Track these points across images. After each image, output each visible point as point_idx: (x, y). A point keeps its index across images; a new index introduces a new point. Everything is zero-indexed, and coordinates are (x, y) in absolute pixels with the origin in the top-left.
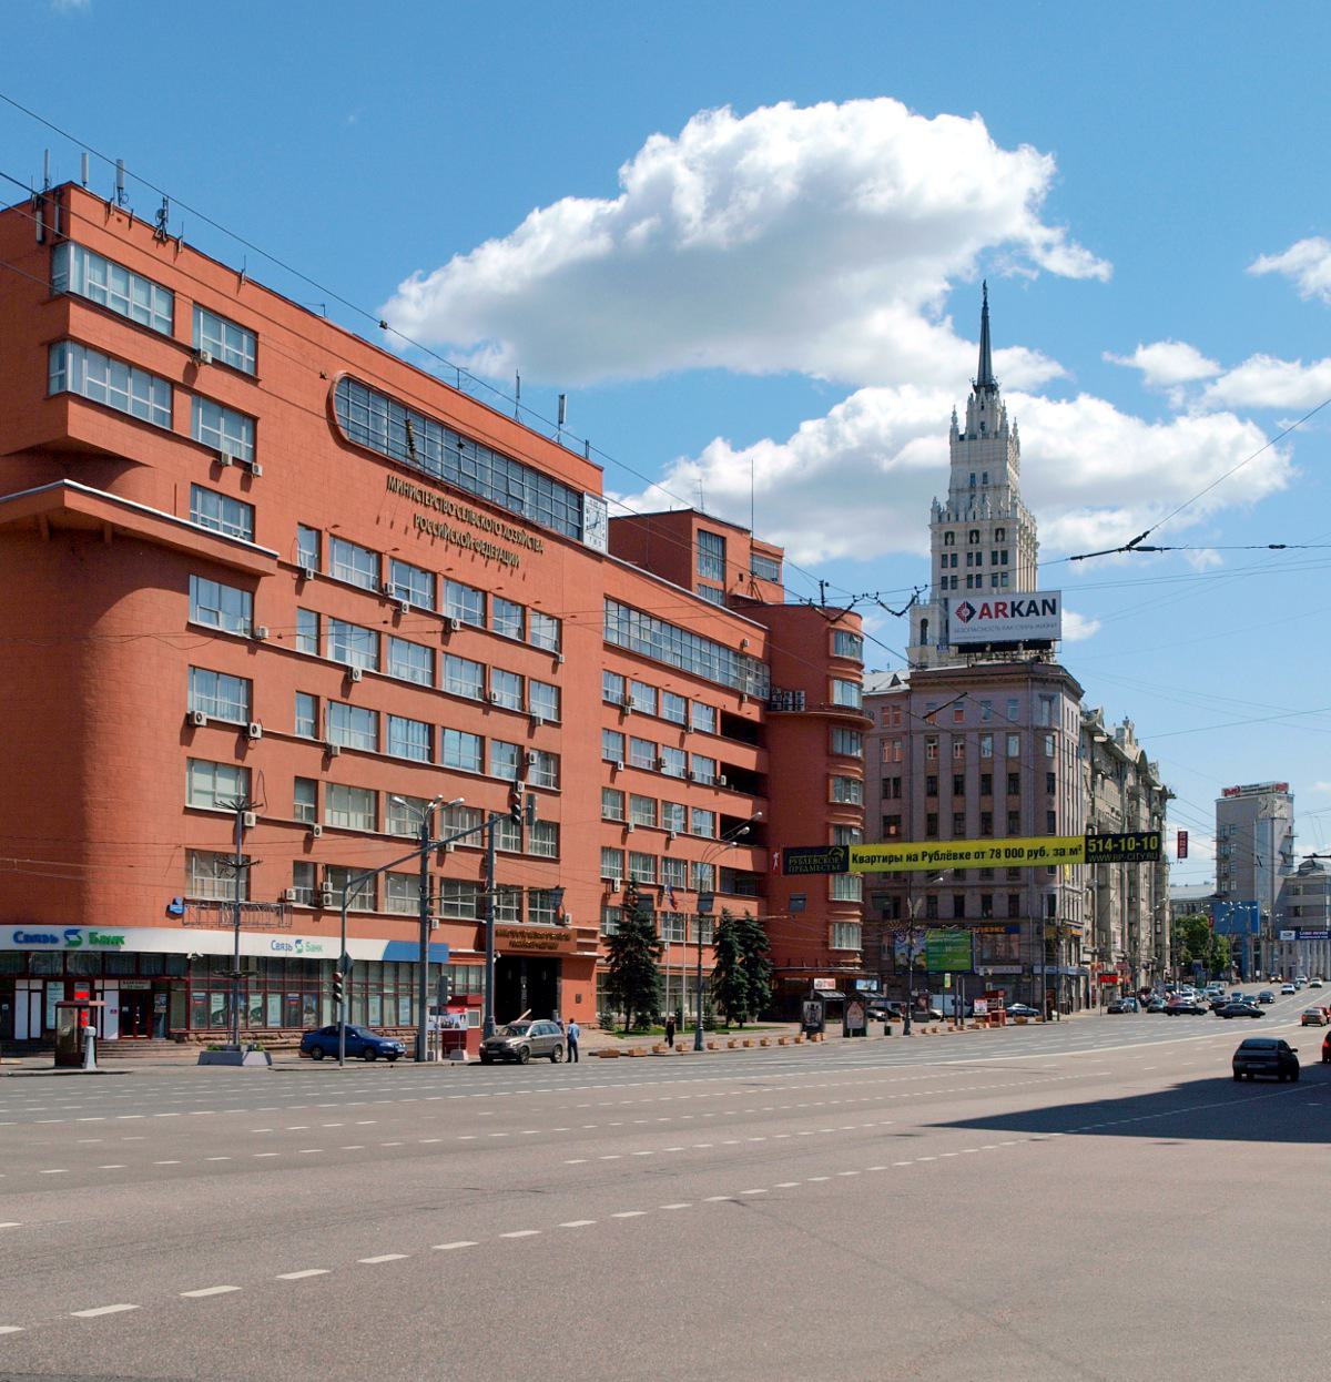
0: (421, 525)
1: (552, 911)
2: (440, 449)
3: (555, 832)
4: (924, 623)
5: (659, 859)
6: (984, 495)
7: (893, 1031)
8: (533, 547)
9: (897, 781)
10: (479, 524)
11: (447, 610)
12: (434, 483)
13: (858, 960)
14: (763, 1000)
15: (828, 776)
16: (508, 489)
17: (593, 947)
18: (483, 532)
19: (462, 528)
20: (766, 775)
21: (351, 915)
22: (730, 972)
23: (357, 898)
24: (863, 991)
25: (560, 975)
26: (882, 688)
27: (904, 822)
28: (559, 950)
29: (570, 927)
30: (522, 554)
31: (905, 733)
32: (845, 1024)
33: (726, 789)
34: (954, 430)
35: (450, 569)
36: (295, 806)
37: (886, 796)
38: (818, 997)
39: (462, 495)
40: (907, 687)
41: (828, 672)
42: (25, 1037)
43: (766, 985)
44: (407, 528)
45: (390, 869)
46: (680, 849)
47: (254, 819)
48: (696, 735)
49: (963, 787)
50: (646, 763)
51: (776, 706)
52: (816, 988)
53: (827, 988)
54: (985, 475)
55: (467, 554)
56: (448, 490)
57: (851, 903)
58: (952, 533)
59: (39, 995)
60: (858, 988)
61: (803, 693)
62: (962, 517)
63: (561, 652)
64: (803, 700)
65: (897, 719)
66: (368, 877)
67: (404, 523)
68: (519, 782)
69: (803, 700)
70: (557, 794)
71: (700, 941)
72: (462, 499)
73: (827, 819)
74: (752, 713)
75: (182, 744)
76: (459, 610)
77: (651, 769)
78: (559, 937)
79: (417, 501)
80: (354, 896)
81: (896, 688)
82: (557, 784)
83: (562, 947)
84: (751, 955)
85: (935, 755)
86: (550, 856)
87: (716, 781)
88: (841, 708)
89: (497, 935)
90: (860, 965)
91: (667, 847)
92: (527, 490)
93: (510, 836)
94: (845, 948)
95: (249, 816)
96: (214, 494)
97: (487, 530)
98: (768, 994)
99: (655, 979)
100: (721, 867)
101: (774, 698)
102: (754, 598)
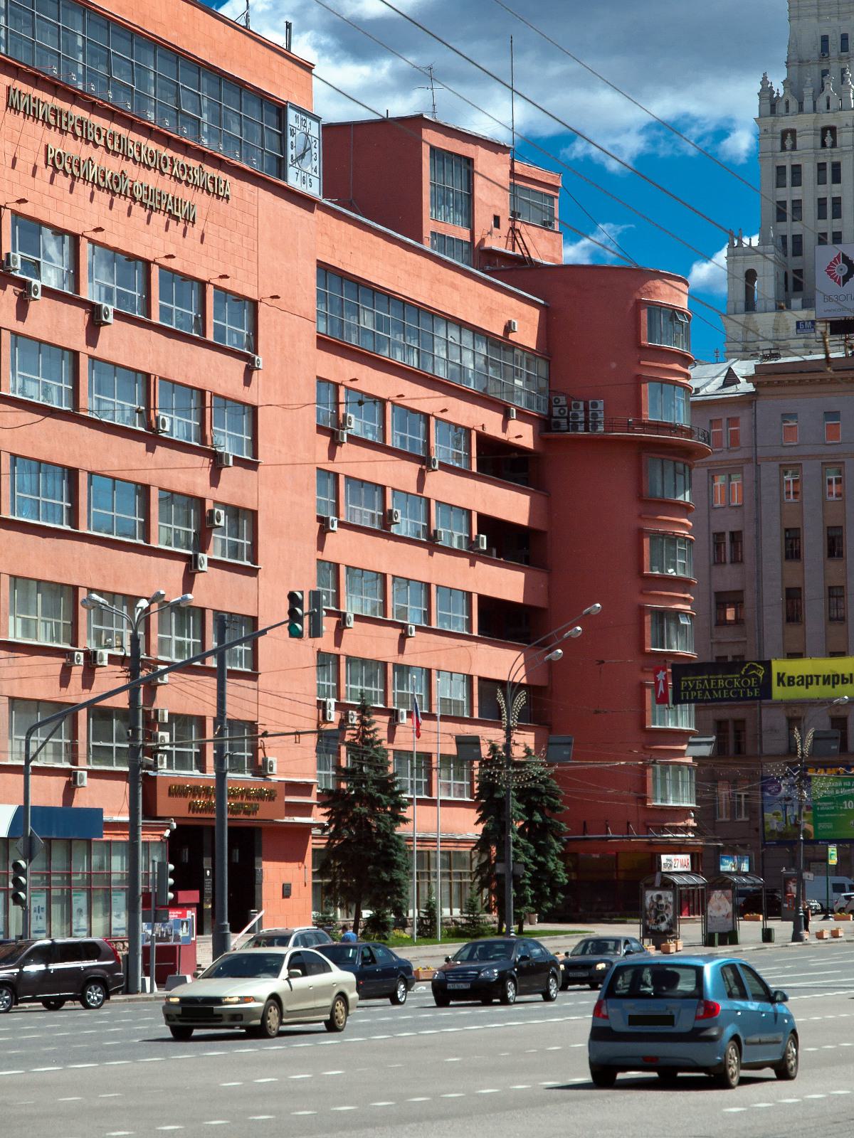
0: (56, 163)
1: (247, 754)
2: (152, 76)
3: (198, 621)
4: (751, 276)
5: (390, 668)
6: (843, 71)
7: (776, 935)
9: (736, 537)
10: (138, 158)
11: (88, 292)
12: (74, 97)
13: (691, 823)
14: (556, 888)
15: (641, 533)
16: (178, 103)
17: (306, 809)
18: (110, 157)
19: (114, 165)
20: (545, 533)
21: (39, 771)
22: (502, 846)
23: (49, 747)
24: (729, 873)
25: (260, 855)
26: (711, 389)
27: (749, 598)
28: (259, 815)
29: (274, 779)
30: (201, 201)
31: (749, 460)
32: (705, 923)
33: (485, 557)
35: (99, 229)
37: (718, 561)
38: (667, 884)
39: (113, 115)
40: (750, 388)
41: (638, 371)
43: (561, 864)
44: (35, 168)
46: (421, 650)
47: (106, 658)
48: (441, 474)
49: (841, 544)
50: (368, 518)
51: (558, 424)
52: (664, 870)
53: (679, 869)
54: (844, 38)
55: (122, 204)
56: (93, 107)
57: (681, 732)
58: (793, 132)
60: (722, 868)
61: (601, 406)
62: (808, 104)
63: (256, 352)
64: (601, 416)
65: (735, 438)
66: (63, 716)
67: (32, 160)
68: (201, 555)
69: (601, 416)
70: (253, 572)
71: (447, 356)
72: (112, 120)
73: (640, 599)
74: (522, 434)
76: (109, 291)
77: (376, 527)
78: (260, 795)
79: (49, 125)
80: (44, 744)
81: (732, 389)
82: (254, 557)
83: (265, 812)
84: (538, 818)
85: (795, 493)
86: (244, 669)
87: (472, 543)
88: (658, 427)
89: (229, 796)
90: (693, 829)
91: (401, 649)
92: (205, 103)
93: (186, 639)
94: (671, 804)
95: (101, 654)
97: (149, 168)
98: (563, 878)
99: (399, 858)
100: (480, 678)
101: (556, 411)
102: (518, 252)
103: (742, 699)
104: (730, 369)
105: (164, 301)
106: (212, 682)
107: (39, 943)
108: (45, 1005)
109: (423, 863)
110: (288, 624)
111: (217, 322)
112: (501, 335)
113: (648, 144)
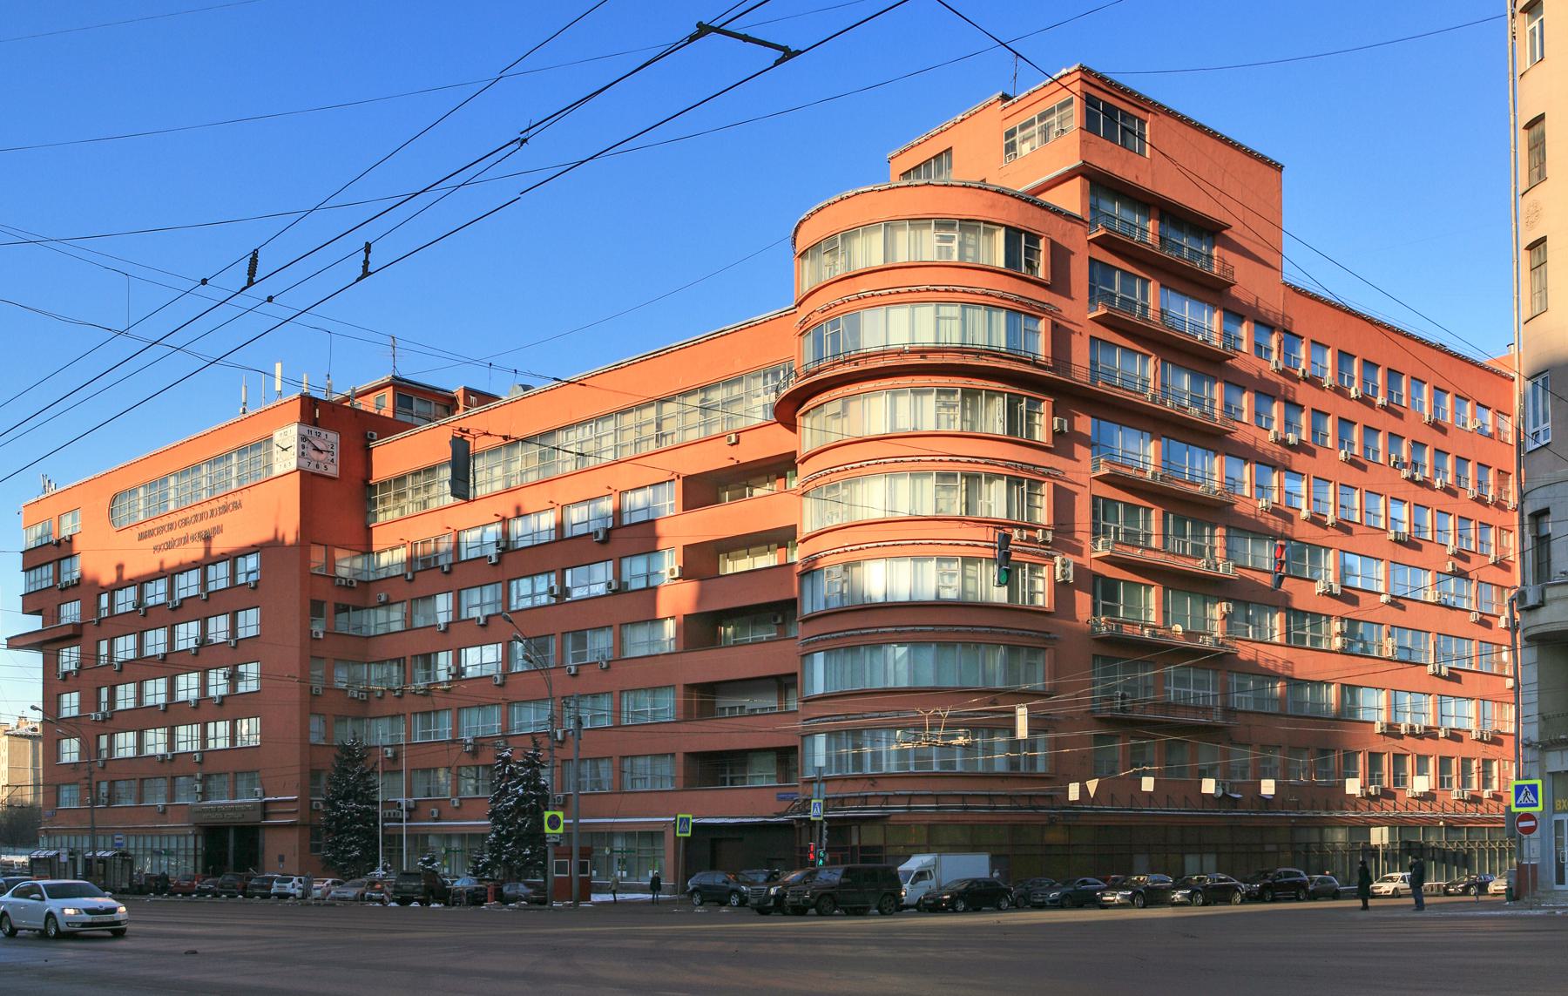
8: (237, 506)
17: (1465, 783)
34: (1054, 431)
36: (312, 801)
42: (195, 726)
45: (1485, 617)
59: (941, 308)
75: (1462, 741)
96: (642, 507)
103: (1022, 778)
104: (1549, 773)
105: (1106, 600)
106: (643, 428)
107: (825, 775)
108: (846, 911)
109: (831, 768)
110: (1169, 366)
111: (1126, 527)
112: (391, 416)
113: (1489, 777)
